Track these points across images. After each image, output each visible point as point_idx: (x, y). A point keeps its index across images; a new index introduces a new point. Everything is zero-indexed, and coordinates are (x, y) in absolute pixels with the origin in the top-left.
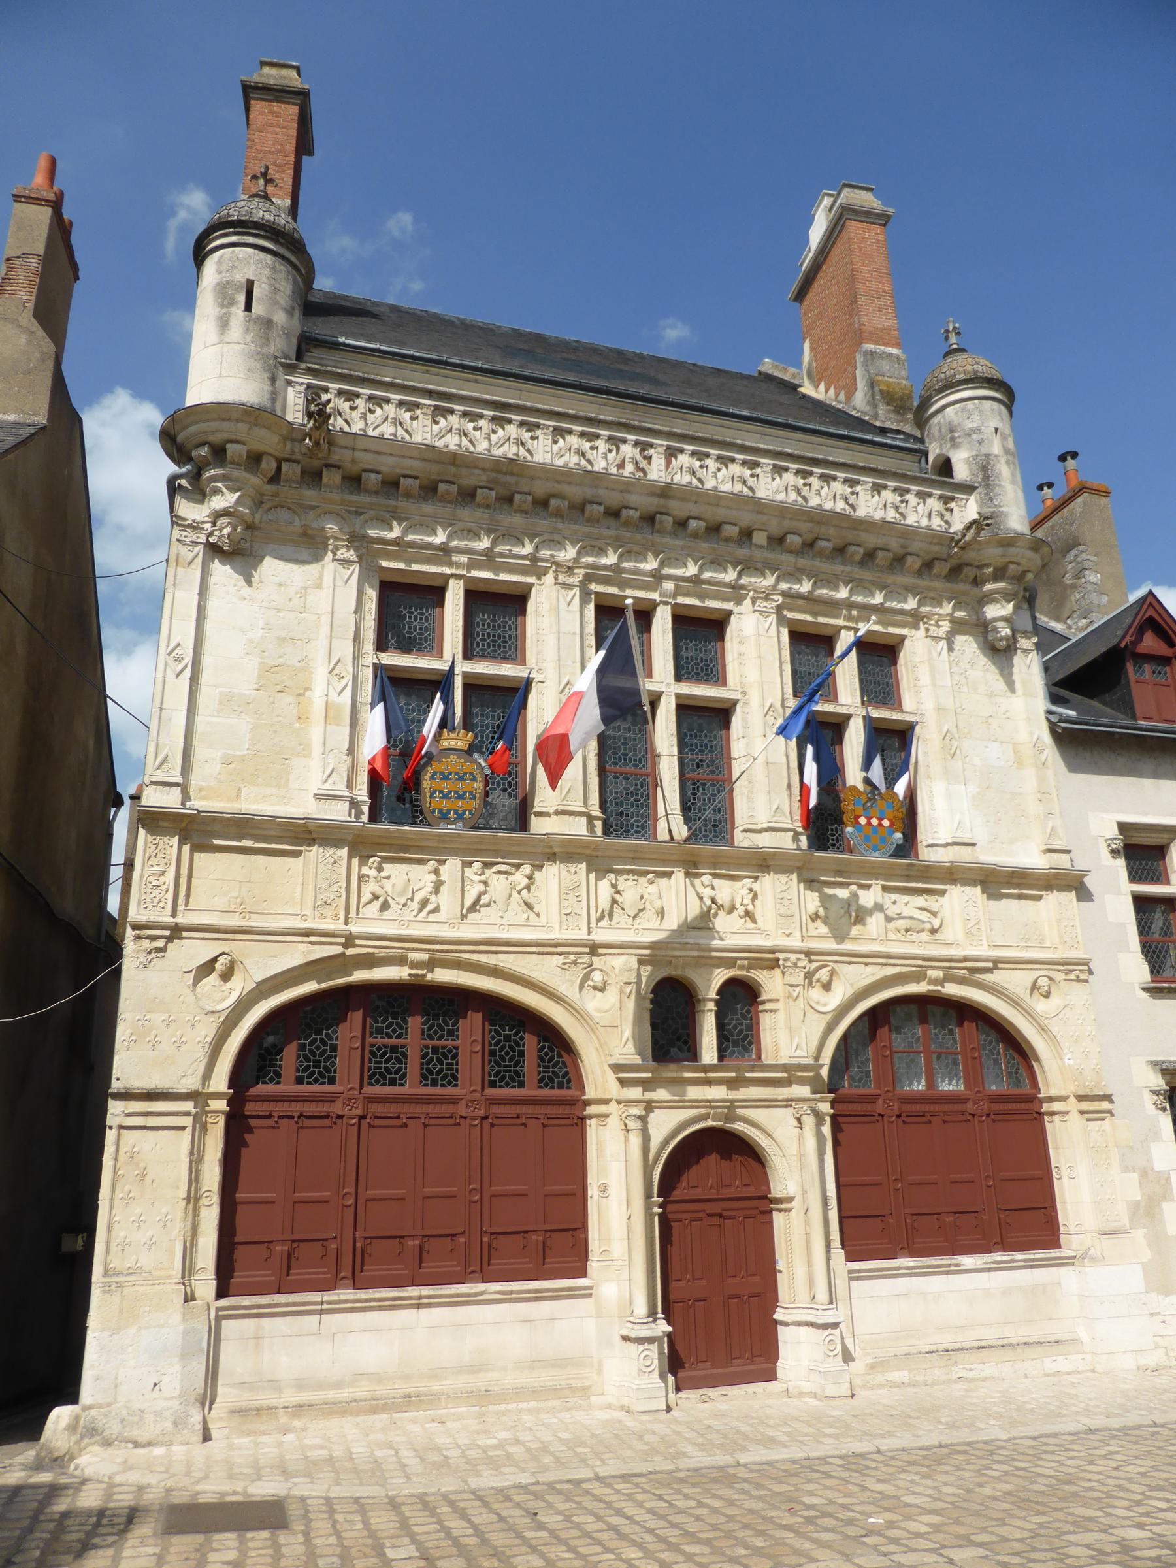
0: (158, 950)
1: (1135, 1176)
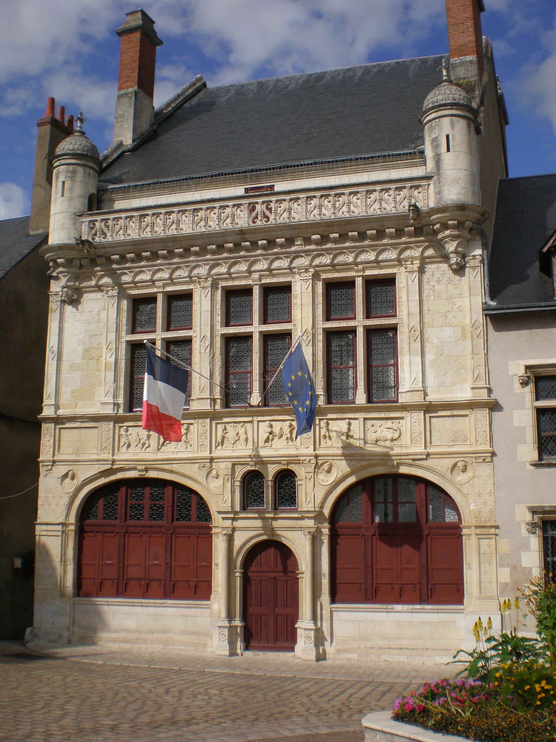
0: (49, 470)
1: (508, 570)
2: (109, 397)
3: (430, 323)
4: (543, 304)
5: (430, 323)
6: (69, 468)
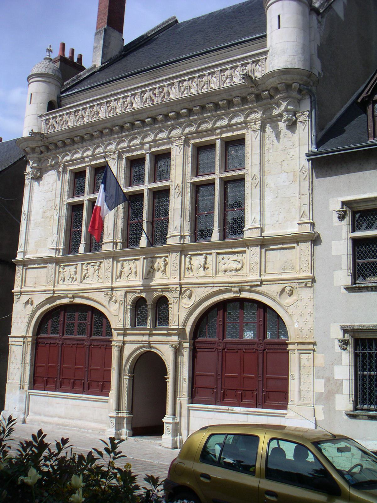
1: (322, 381)
2: (54, 245)
3: (269, 171)
4: (353, 146)
5: (269, 171)
6: (29, 296)
